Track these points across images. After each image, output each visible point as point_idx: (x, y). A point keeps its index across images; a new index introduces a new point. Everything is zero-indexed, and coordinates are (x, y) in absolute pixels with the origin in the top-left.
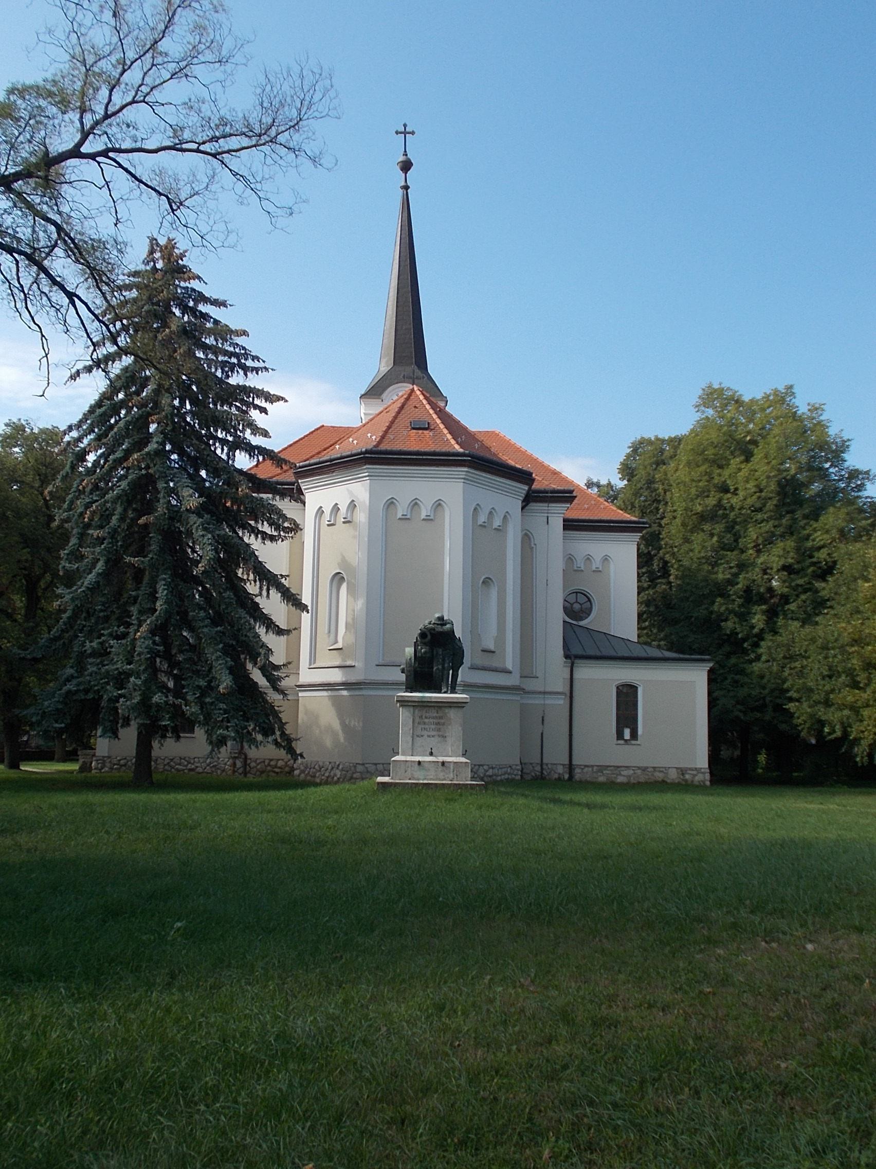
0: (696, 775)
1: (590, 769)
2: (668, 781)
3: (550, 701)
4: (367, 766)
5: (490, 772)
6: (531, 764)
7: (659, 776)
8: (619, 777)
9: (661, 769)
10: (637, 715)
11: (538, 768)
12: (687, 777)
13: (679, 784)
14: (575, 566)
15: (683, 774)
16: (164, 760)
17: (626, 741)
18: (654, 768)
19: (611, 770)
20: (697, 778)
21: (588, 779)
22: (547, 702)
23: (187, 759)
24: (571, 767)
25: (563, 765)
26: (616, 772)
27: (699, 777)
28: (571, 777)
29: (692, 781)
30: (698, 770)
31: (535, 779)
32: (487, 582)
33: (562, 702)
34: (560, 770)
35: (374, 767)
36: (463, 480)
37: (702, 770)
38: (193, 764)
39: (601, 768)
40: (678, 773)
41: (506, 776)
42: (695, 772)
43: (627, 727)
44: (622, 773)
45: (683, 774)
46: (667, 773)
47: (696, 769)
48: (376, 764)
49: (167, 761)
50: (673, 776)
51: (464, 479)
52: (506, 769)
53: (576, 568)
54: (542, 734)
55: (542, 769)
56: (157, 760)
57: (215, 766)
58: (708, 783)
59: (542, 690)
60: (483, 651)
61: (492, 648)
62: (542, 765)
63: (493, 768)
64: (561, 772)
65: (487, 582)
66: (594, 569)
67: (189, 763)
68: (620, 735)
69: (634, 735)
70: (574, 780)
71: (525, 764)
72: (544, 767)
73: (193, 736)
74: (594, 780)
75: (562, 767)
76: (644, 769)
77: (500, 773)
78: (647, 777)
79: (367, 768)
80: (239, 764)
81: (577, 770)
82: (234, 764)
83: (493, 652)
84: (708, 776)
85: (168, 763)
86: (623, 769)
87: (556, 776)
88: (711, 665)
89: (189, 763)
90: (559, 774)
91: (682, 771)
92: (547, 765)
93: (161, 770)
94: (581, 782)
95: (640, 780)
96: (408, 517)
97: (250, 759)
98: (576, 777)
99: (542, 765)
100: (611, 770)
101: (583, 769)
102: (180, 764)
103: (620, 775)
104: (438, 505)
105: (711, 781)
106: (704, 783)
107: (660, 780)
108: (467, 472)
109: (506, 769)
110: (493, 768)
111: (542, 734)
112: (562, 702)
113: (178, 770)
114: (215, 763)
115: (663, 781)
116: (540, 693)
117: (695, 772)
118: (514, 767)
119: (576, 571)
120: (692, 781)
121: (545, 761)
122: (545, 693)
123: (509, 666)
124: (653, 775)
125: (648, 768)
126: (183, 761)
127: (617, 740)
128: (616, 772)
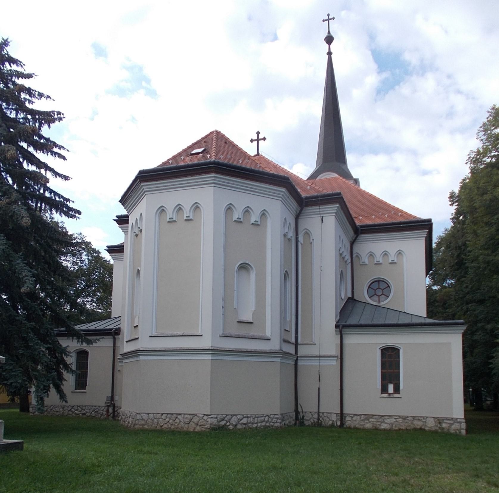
0: (453, 424)
1: (359, 417)
2: (427, 429)
3: (325, 363)
4: (142, 415)
5: (245, 421)
6: (311, 412)
7: (418, 424)
8: (382, 424)
9: (420, 419)
10: (399, 373)
11: (316, 416)
12: (444, 425)
13: (436, 432)
14: (361, 261)
15: (440, 423)
16: (68, 407)
17: (390, 394)
18: (414, 417)
19: (375, 418)
20: (453, 427)
21: (357, 426)
22: (321, 364)
23: (81, 407)
24: (342, 415)
25: (337, 414)
26: (380, 420)
27: (456, 426)
28: (342, 424)
29: (448, 430)
30: (455, 420)
31: (314, 425)
32: (244, 267)
33: (334, 363)
34: (334, 418)
35: (147, 415)
36: (213, 185)
37: (458, 420)
38: (84, 410)
39: (368, 417)
40: (435, 422)
41: (264, 424)
42: (451, 422)
43: (391, 383)
44: (386, 421)
45: (440, 423)
46: (425, 422)
47: (452, 418)
48: (148, 414)
49: (70, 408)
50: (431, 424)
51: (214, 183)
52: (263, 418)
53: (361, 263)
54: (319, 389)
55: (319, 415)
56: (64, 407)
57: (97, 411)
58: (464, 432)
59: (317, 354)
60: (238, 322)
61: (251, 321)
62: (319, 413)
63: (248, 417)
64: (335, 420)
65: (244, 267)
66: (376, 262)
67: (82, 409)
68: (384, 389)
69: (397, 390)
70: (345, 426)
71: (306, 412)
72: (321, 415)
73: (84, 391)
74: (362, 427)
75: (335, 415)
76: (405, 418)
77: (256, 421)
78: (406, 425)
79: (142, 416)
80: (111, 410)
81: (348, 418)
82: (108, 411)
83: (252, 323)
84: (464, 426)
85: (71, 409)
86: (386, 417)
87: (330, 422)
88: (465, 328)
89: (82, 409)
90: (333, 421)
91: (440, 421)
92: (323, 413)
93: (66, 414)
94: (349, 428)
95: (402, 428)
96: (174, 219)
97: (118, 407)
98: (347, 424)
99: (319, 413)
100: (375, 418)
101: (352, 417)
102: (77, 410)
103: (384, 422)
104: (196, 207)
105: (467, 431)
106: (460, 432)
107: (418, 427)
108: (214, 177)
109: (263, 418)
110: (248, 417)
111: (319, 389)
112: (335, 363)
113: (76, 414)
114: (97, 410)
115: (421, 429)
116: (316, 356)
117: (451, 422)
118: (272, 416)
119: (361, 265)
120: (448, 430)
121: (321, 411)
122: (320, 356)
123: (268, 334)
124: (412, 423)
125: (408, 417)
126: (79, 408)
127: (382, 393)
128: (380, 420)
